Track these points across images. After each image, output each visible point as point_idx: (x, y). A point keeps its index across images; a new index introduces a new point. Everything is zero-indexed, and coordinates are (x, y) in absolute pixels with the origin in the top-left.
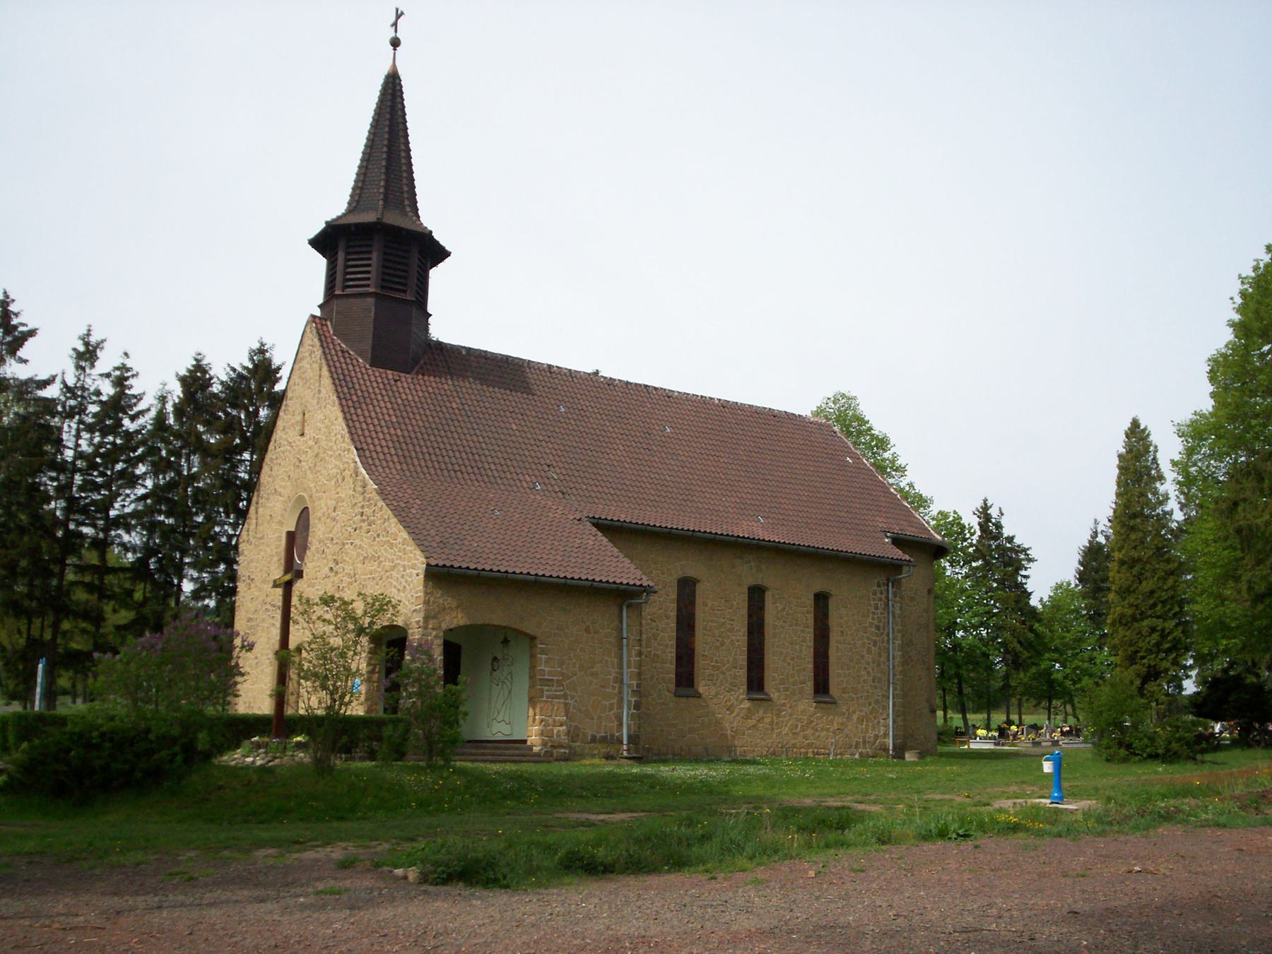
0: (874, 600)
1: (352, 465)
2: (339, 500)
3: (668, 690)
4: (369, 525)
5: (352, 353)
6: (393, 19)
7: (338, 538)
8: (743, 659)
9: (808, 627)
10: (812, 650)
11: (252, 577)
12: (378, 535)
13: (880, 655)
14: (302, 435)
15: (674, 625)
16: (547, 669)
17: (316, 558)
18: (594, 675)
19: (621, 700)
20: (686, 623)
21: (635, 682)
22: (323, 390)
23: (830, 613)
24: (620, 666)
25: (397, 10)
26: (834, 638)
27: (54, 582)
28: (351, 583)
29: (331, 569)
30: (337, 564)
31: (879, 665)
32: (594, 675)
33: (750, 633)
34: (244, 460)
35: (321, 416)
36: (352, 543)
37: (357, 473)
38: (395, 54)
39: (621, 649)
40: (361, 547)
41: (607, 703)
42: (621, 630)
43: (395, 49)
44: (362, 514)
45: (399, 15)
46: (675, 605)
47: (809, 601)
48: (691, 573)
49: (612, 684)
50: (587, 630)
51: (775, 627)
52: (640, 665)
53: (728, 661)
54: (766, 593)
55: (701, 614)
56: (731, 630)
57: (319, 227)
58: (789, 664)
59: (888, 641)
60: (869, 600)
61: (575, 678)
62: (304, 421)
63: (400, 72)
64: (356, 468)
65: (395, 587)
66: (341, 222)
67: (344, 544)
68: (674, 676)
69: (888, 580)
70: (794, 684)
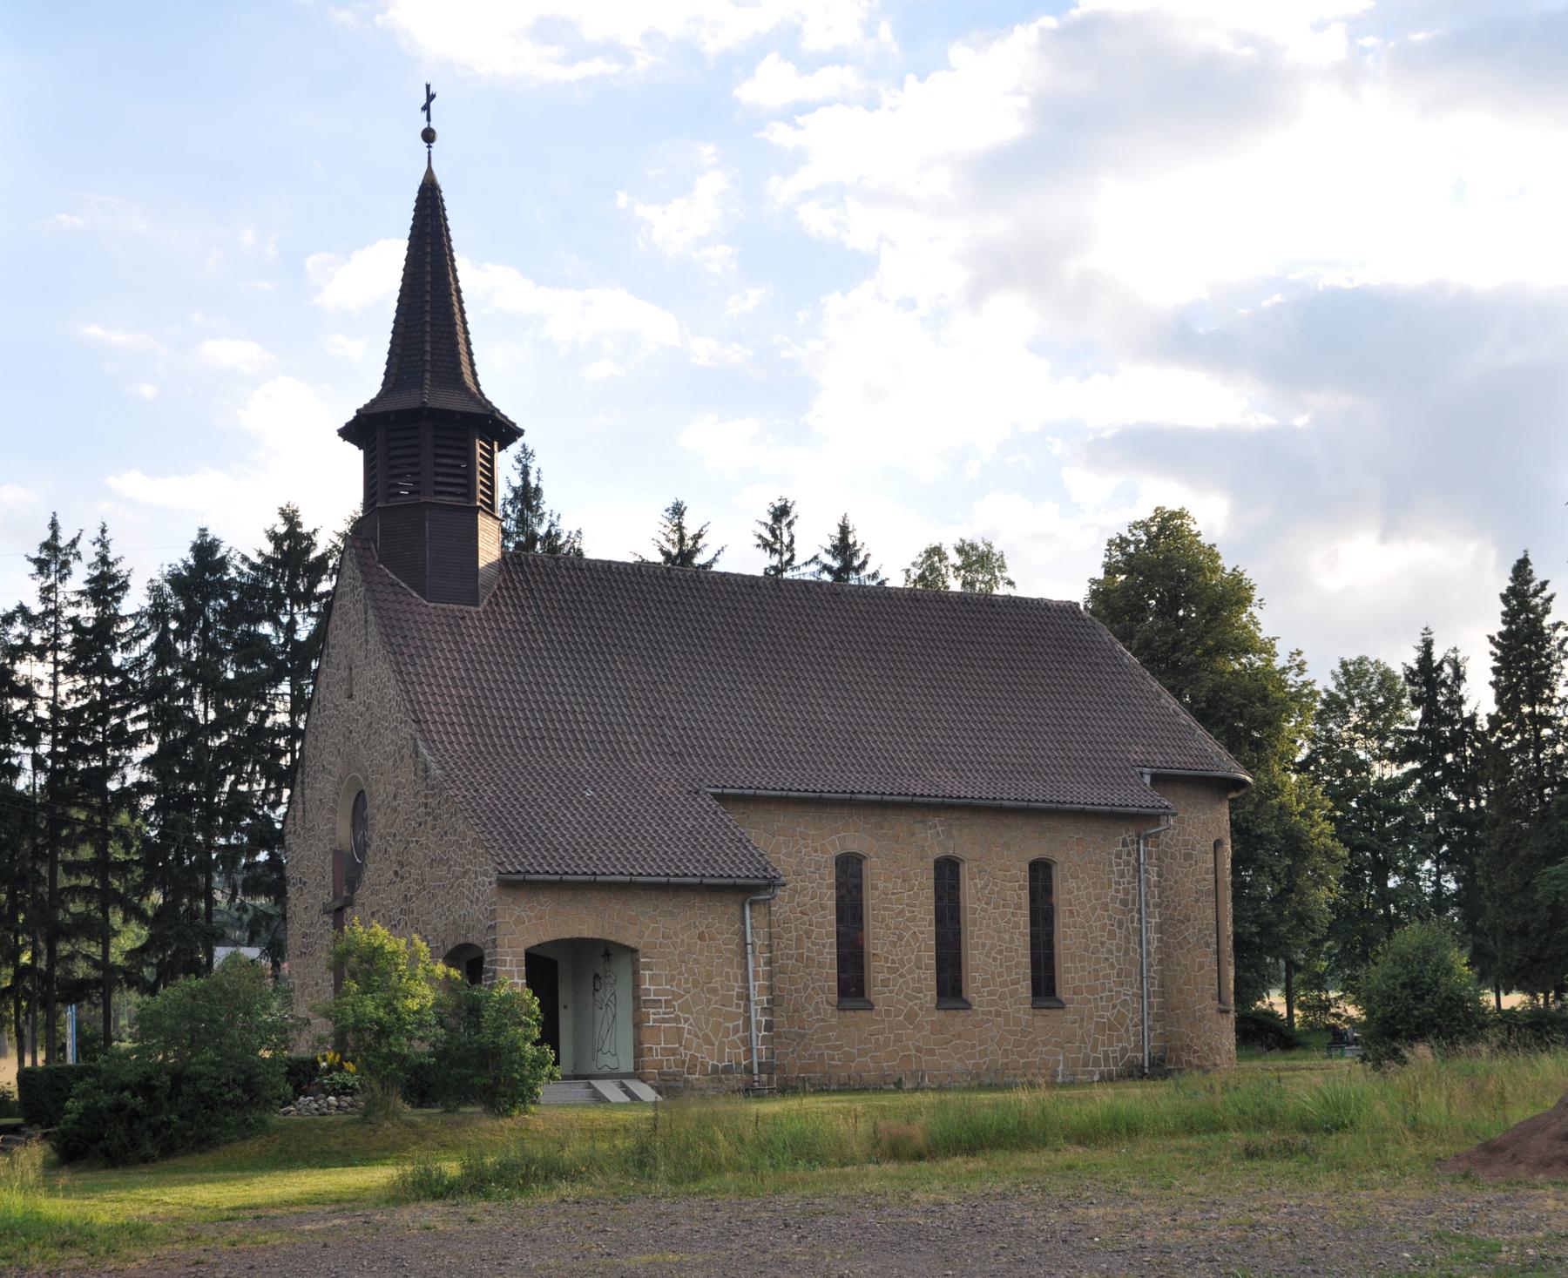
0: (1118, 864)
1: (411, 743)
2: (398, 785)
3: (829, 1003)
4: (435, 819)
5: (403, 585)
6: (432, 104)
7: (401, 834)
8: (929, 957)
9: (1021, 908)
10: (1028, 938)
11: (304, 879)
12: (446, 833)
13: (1128, 941)
14: (350, 697)
15: (833, 917)
16: (652, 988)
17: (378, 858)
18: (714, 991)
19: (748, 1021)
20: (850, 911)
21: (765, 998)
22: (372, 642)
23: (1054, 885)
24: (746, 979)
25: (428, 87)
26: (1061, 920)
27: (44, 890)
28: (418, 892)
29: (396, 873)
30: (402, 866)
31: (1126, 953)
32: (714, 991)
33: (939, 921)
34: (282, 695)
35: (369, 674)
36: (417, 842)
37: (417, 753)
39: (745, 957)
40: (428, 847)
41: (731, 1025)
42: (745, 933)
44: (426, 805)
45: (430, 97)
46: (834, 891)
47: (1023, 874)
48: (853, 847)
49: (735, 1001)
50: (701, 937)
51: (974, 911)
52: (770, 976)
53: (909, 961)
54: (961, 867)
55: (872, 900)
56: (913, 919)
57: (350, 415)
58: (995, 959)
59: (1140, 921)
60: (1111, 865)
61: (688, 996)
62: (351, 679)
63: (441, 179)
64: (416, 746)
65: (468, 898)
66: (376, 410)
67: (408, 843)
68: (835, 984)
69: (1138, 836)
70: (1003, 984)
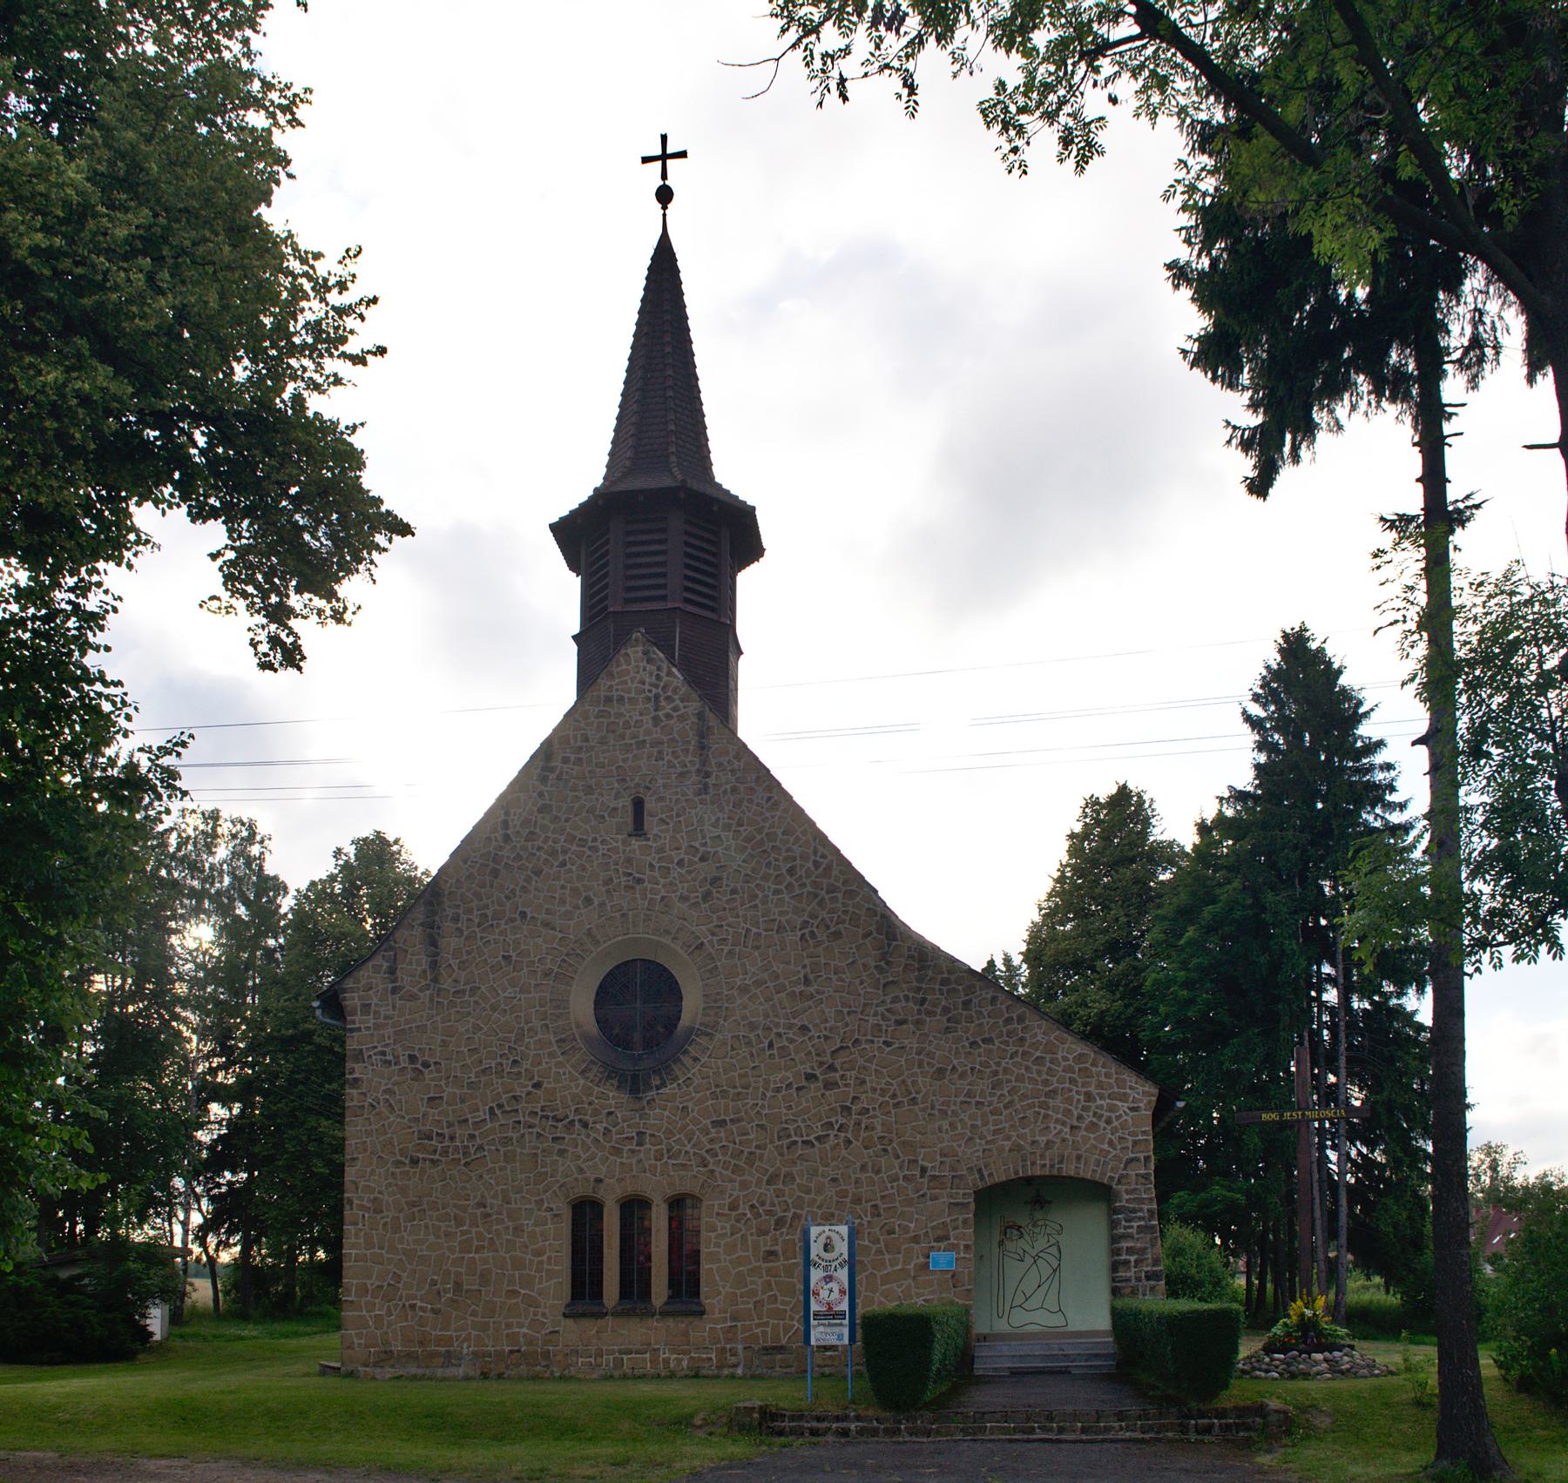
38: (664, 215)
43: (665, 208)
